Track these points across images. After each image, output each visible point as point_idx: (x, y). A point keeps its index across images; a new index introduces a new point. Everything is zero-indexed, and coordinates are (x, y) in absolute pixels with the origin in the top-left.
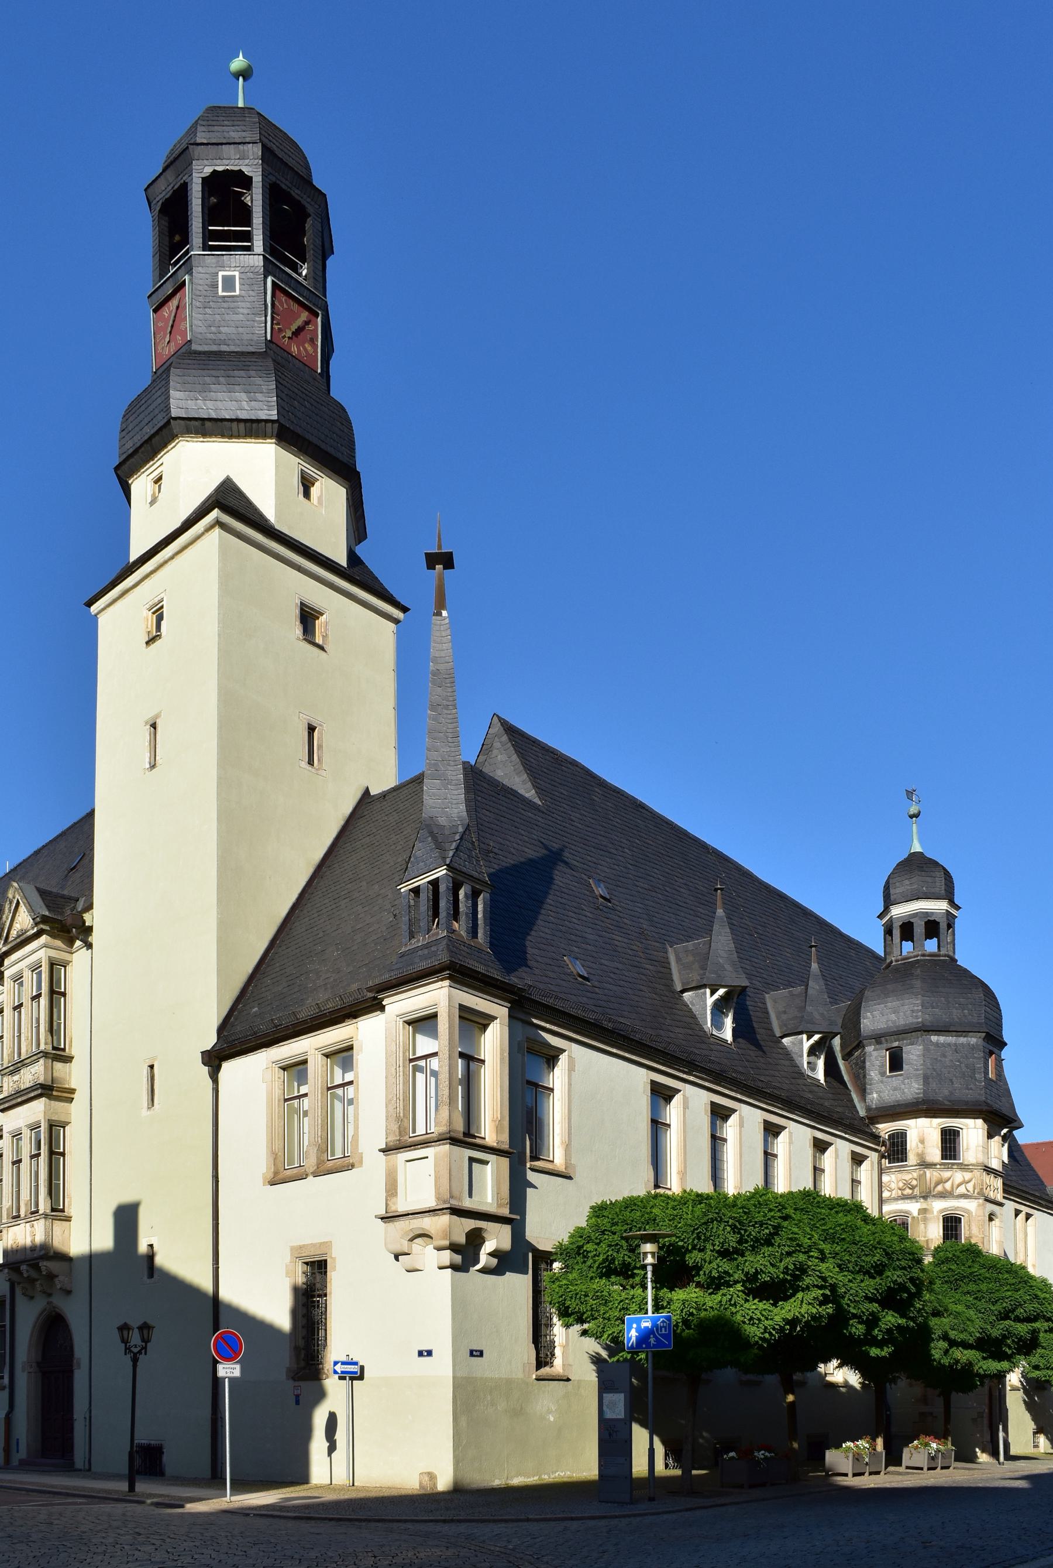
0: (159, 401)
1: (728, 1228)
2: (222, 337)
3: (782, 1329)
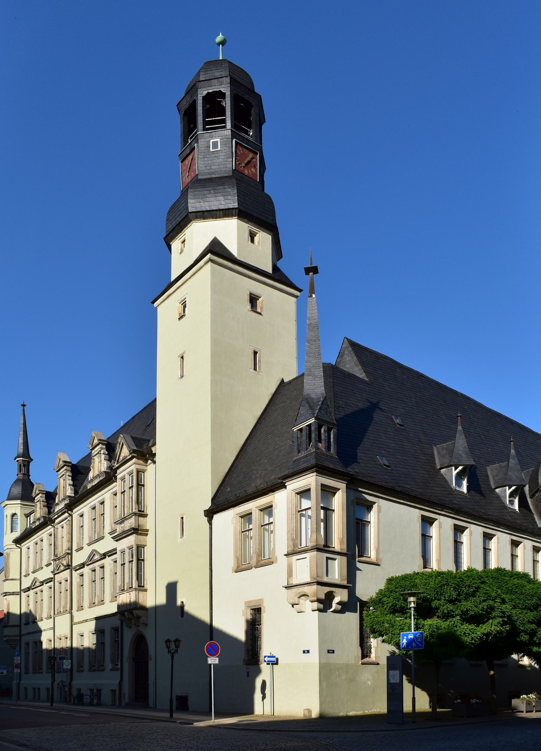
0: (183, 205)
1: (452, 589)
2: (212, 171)
3: (481, 638)
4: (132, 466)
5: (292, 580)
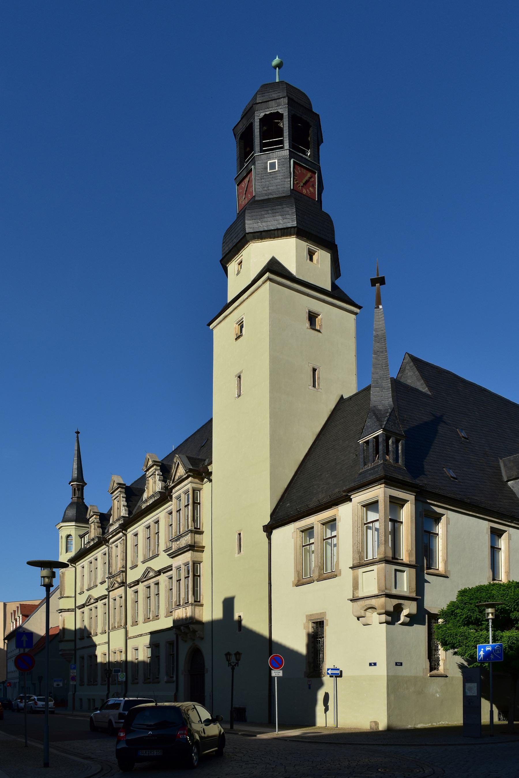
0: (240, 226)
2: (269, 191)
4: (188, 485)
5: (357, 593)
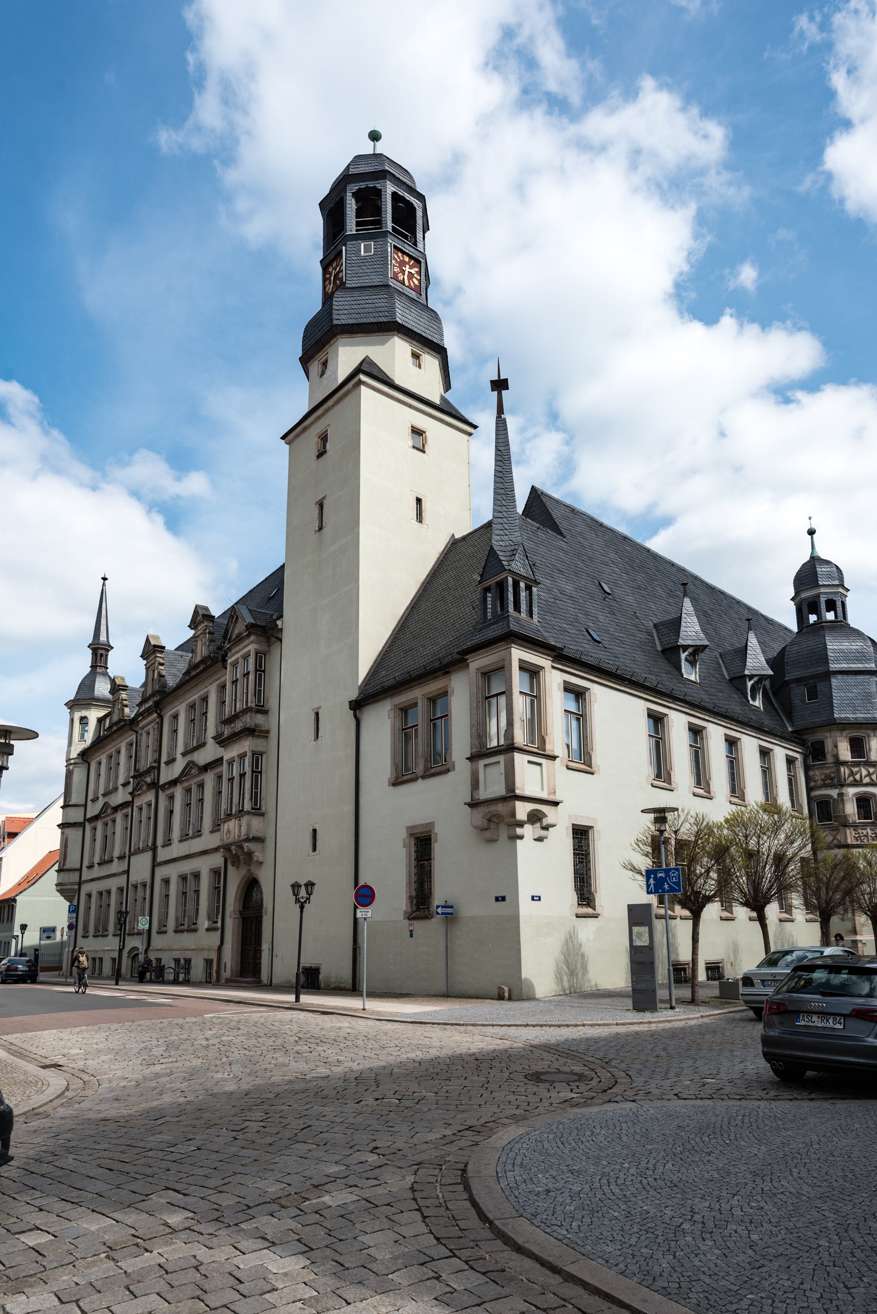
5: (478, 794)
